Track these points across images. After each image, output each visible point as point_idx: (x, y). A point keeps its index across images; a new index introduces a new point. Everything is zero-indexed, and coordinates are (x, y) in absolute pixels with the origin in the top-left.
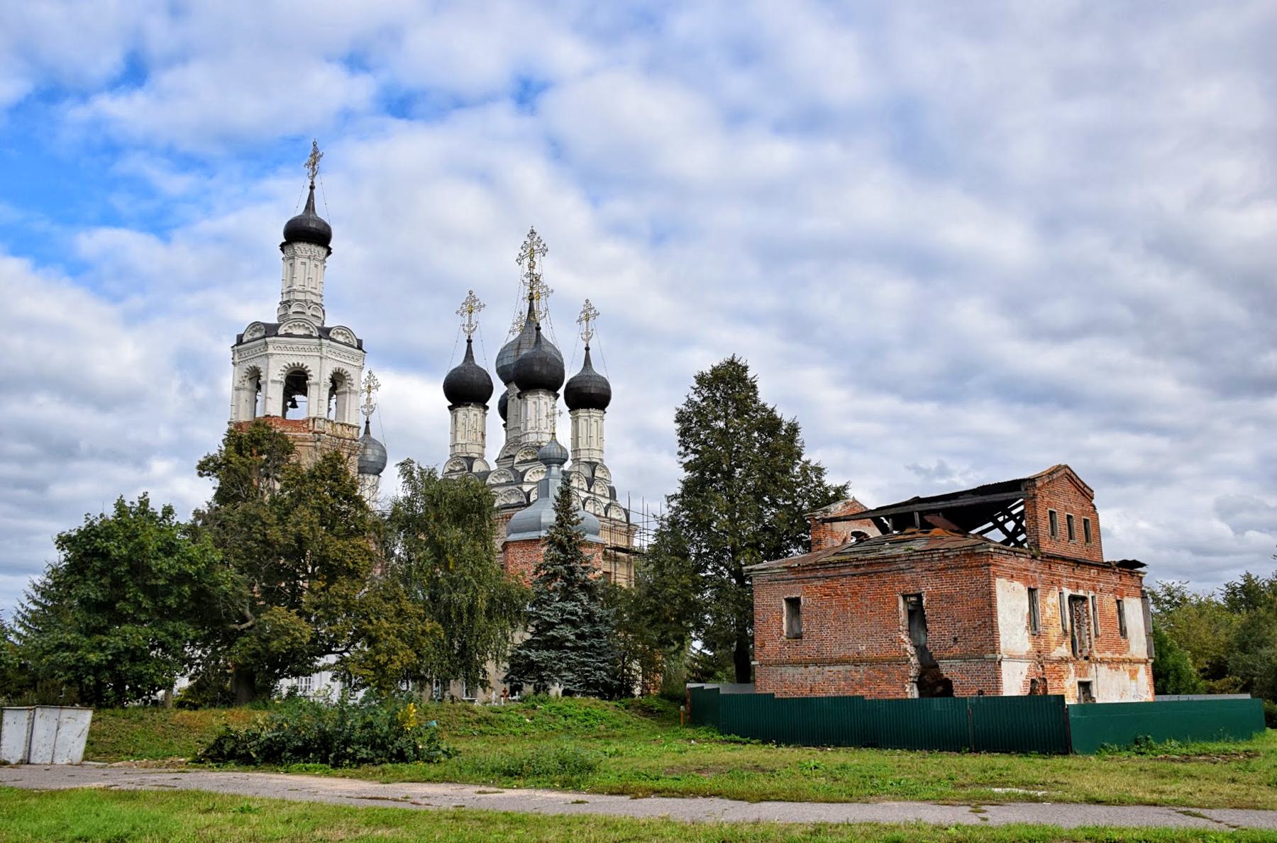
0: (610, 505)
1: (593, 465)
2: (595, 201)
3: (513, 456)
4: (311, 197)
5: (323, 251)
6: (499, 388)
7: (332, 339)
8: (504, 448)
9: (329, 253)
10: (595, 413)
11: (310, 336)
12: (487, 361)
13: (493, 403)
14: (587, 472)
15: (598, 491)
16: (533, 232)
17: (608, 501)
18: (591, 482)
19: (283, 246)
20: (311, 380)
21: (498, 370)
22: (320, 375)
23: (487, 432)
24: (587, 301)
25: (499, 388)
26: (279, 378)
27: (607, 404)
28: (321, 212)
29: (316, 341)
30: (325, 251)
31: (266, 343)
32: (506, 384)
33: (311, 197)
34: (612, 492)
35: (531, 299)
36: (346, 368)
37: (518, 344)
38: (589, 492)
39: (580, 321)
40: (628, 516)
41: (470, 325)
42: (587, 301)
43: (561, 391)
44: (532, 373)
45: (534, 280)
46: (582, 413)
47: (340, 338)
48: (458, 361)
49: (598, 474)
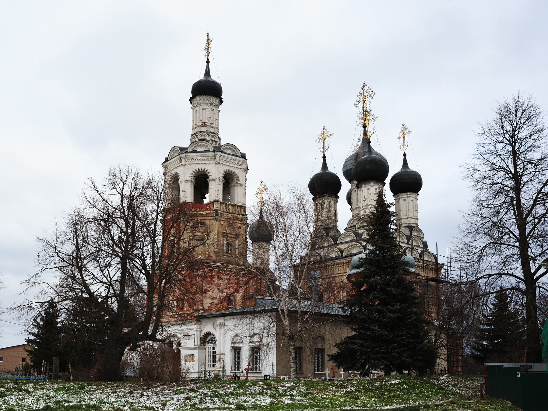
0: (423, 252)
1: (411, 228)
2: (417, 224)
3: (355, 226)
4: (208, 67)
5: (215, 100)
6: (346, 186)
7: (222, 152)
8: (351, 220)
9: (221, 102)
10: (412, 195)
11: (208, 151)
12: (336, 168)
13: (343, 194)
14: (407, 232)
15: (414, 244)
16: (364, 85)
17: (422, 250)
18: (409, 238)
19: (191, 99)
20: (211, 178)
21: (344, 174)
22: (216, 173)
23: (338, 212)
24: (403, 125)
25: (346, 186)
26: (190, 179)
27: (420, 189)
28: (214, 77)
29: (212, 153)
30: (218, 101)
31: (180, 158)
32: (350, 181)
33: (208, 67)
34: (425, 245)
35: (365, 127)
36: (234, 170)
37: (356, 156)
38: (408, 244)
39: (399, 138)
40: (436, 259)
41: (324, 147)
42: (403, 125)
43: (387, 181)
44: (367, 168)
45: (366, 112)
46: (403, 196)
47: (229, 151)
48: (318, 169)
49: (414, 233)
